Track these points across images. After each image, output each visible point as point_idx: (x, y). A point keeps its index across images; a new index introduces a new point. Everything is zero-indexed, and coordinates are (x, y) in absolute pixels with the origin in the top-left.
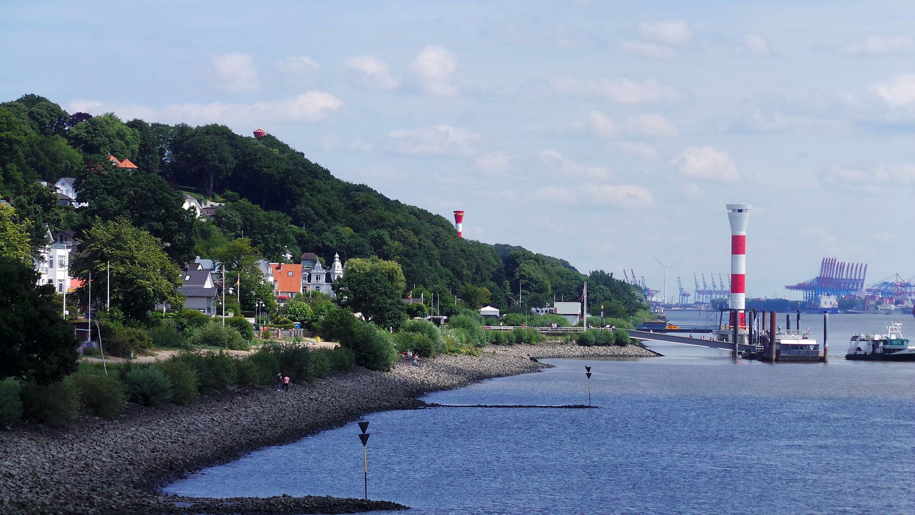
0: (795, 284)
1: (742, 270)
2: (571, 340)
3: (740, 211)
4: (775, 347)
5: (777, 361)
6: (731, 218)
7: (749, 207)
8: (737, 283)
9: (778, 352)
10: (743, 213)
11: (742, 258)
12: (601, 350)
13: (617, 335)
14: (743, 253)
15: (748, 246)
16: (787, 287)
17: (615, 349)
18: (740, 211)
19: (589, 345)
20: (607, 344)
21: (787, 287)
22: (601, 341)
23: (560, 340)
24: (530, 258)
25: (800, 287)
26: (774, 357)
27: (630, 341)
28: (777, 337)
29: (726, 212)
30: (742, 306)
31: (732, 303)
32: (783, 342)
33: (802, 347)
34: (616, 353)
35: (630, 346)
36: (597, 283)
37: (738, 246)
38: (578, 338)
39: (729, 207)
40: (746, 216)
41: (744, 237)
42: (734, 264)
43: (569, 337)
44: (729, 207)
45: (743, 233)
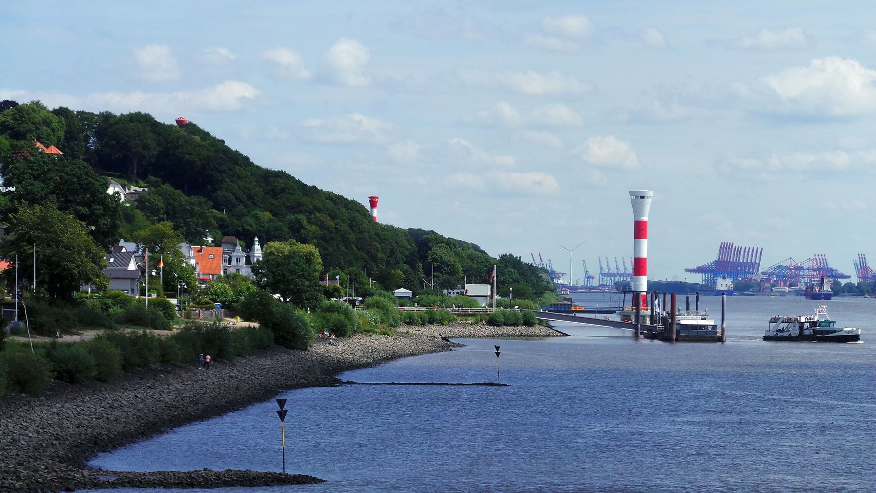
0: (694, 266)
1: (644, 254)
2: (481, 321)
3: (643, 197)
4: (675, 327)
5: (677, 340)
8: (639, 266)
9: (678, 332)
11: (644, 243)
12: (509, 330)
14: (645, 237)
15: (650, 230)
16: (687, 270)
17: (523, 329)
18: (643, 197)
19: (498, 326)
20: (516, 324)
21: (687, 270)
22: (510, 322)
23: (471, 320)
24: (442, 242)
25: (700, 270)
28: (677, 318)
29: (629, 198)
32: (682, 322)
36: (506, 266)
37: (640, 230)
38: (488, 318)
39: (631, 193)
42: (637, 248)
43: (479, 317)
44: (631, 193)
45: (645, 218)
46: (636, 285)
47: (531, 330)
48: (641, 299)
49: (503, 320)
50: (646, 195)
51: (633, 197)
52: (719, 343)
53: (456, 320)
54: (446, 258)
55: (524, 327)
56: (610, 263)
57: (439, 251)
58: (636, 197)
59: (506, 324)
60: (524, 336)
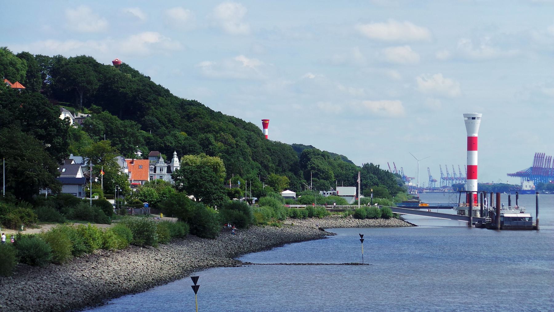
0: (514, 172)
1: (475, 163)
2: (349, 215)
3: (474, 118)
4: (500, 219)
5: (501, 229)
6: (466, 122)
7: (480, 115)
8: (472, 172)
9: (502, 223)
10: (476, 120)
11: (475, 153)
12: (371, 222)
14: (476, 149)
16: (509, 175)
17: (381, 221)
18: (474, 118)
19: (362, 219)
20: (375, 217)
21: (509, 175)
23: (341, 214)
24: (319, 154)
26: (499, 226)
27: (392, 215)
29: (463, 119)
30: (475, 188)
31: (468, 186)
32: (505, 215)
34: (382, 224)
36: (368, 173)
37: (472, 144)
38: (354, 213)
39: (465, 115)
40: (478, 122)
41: (476, 138)
42: (469, 158)
43: (347, 212)
44: (465, 115)
45: (476, 135)
47: (387, 222)
49: (366, 214)
50: (476, 117)
51: (466, 119)
52: (535, 231)
53: (329, 214)
54: (321, 167)
55: (382, 220)
56: (442, 170)
57: (317, 162)
59: (368, 218)
60: (382, 226)
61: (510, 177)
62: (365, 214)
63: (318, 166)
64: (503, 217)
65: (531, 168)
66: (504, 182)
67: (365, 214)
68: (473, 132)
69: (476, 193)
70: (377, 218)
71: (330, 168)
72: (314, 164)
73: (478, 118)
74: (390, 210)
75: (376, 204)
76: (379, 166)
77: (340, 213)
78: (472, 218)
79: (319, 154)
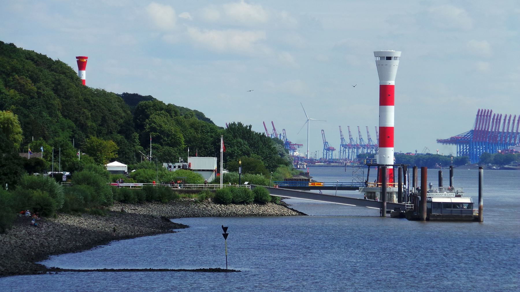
0: (447, 137)
1: (391, 123)
2: (207, 198)
3: (389, 58)
4: (426, 206)
5: (428, 220)
6: (378, 64)
7: (398, 54)
8: (386, 136)
9: (429, 211)
10: (393, 61)
11: (391, 110)
13: (256, 192)
14: (392, 104)
15: (397, 96)
16: (439, 141)
17: (254, 208)
18: (389, 58)
19: (225, 204)
20: (244, 202)
21: (439, 141)
24: (161, 109)
25: (454, 141)
26: (425, 216)
27: (270, 199)
31: (380, 157)
32: (434, 200)
33: (455, 205)
35: (270, 204)
36: (235, 137)
37: (386, 96)
38: (214, 195)
39: (376, 54)
40: (395, 64)
41: (392, 87)
42: (382, 116)
43: (204, 194)
44: (376, 54)
45: (392, 82)
46: (382, 158)
47: (263, 209)
48: (387, 173)
50: (393, 56)
51: (378, 59)
54: (166, 127)
57: (158, 119)
58: (382, 58)
59: (234, 202)
60: (255, 215)
61: (441, 144)
62: (231, 196)
63: (161, 126)
64: (431, 202)
65: (472, 131)
66: (433, 152)
67: (231, 196)
68: (388, 78)
69: (392, 167)
70: (248, 204)
71: (178, 129)
72: (155, 123)
73: (396, 58)
74: (267, 191)
75: (246, 183)
76: (250, 127)
77: (194, 195)
78: (385, 204)
79: (161, 109)
